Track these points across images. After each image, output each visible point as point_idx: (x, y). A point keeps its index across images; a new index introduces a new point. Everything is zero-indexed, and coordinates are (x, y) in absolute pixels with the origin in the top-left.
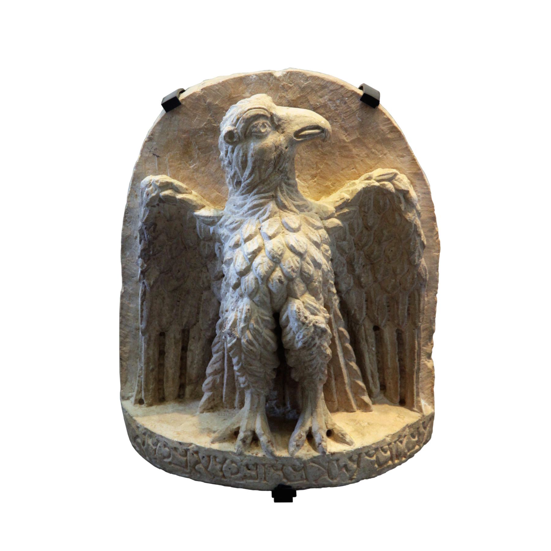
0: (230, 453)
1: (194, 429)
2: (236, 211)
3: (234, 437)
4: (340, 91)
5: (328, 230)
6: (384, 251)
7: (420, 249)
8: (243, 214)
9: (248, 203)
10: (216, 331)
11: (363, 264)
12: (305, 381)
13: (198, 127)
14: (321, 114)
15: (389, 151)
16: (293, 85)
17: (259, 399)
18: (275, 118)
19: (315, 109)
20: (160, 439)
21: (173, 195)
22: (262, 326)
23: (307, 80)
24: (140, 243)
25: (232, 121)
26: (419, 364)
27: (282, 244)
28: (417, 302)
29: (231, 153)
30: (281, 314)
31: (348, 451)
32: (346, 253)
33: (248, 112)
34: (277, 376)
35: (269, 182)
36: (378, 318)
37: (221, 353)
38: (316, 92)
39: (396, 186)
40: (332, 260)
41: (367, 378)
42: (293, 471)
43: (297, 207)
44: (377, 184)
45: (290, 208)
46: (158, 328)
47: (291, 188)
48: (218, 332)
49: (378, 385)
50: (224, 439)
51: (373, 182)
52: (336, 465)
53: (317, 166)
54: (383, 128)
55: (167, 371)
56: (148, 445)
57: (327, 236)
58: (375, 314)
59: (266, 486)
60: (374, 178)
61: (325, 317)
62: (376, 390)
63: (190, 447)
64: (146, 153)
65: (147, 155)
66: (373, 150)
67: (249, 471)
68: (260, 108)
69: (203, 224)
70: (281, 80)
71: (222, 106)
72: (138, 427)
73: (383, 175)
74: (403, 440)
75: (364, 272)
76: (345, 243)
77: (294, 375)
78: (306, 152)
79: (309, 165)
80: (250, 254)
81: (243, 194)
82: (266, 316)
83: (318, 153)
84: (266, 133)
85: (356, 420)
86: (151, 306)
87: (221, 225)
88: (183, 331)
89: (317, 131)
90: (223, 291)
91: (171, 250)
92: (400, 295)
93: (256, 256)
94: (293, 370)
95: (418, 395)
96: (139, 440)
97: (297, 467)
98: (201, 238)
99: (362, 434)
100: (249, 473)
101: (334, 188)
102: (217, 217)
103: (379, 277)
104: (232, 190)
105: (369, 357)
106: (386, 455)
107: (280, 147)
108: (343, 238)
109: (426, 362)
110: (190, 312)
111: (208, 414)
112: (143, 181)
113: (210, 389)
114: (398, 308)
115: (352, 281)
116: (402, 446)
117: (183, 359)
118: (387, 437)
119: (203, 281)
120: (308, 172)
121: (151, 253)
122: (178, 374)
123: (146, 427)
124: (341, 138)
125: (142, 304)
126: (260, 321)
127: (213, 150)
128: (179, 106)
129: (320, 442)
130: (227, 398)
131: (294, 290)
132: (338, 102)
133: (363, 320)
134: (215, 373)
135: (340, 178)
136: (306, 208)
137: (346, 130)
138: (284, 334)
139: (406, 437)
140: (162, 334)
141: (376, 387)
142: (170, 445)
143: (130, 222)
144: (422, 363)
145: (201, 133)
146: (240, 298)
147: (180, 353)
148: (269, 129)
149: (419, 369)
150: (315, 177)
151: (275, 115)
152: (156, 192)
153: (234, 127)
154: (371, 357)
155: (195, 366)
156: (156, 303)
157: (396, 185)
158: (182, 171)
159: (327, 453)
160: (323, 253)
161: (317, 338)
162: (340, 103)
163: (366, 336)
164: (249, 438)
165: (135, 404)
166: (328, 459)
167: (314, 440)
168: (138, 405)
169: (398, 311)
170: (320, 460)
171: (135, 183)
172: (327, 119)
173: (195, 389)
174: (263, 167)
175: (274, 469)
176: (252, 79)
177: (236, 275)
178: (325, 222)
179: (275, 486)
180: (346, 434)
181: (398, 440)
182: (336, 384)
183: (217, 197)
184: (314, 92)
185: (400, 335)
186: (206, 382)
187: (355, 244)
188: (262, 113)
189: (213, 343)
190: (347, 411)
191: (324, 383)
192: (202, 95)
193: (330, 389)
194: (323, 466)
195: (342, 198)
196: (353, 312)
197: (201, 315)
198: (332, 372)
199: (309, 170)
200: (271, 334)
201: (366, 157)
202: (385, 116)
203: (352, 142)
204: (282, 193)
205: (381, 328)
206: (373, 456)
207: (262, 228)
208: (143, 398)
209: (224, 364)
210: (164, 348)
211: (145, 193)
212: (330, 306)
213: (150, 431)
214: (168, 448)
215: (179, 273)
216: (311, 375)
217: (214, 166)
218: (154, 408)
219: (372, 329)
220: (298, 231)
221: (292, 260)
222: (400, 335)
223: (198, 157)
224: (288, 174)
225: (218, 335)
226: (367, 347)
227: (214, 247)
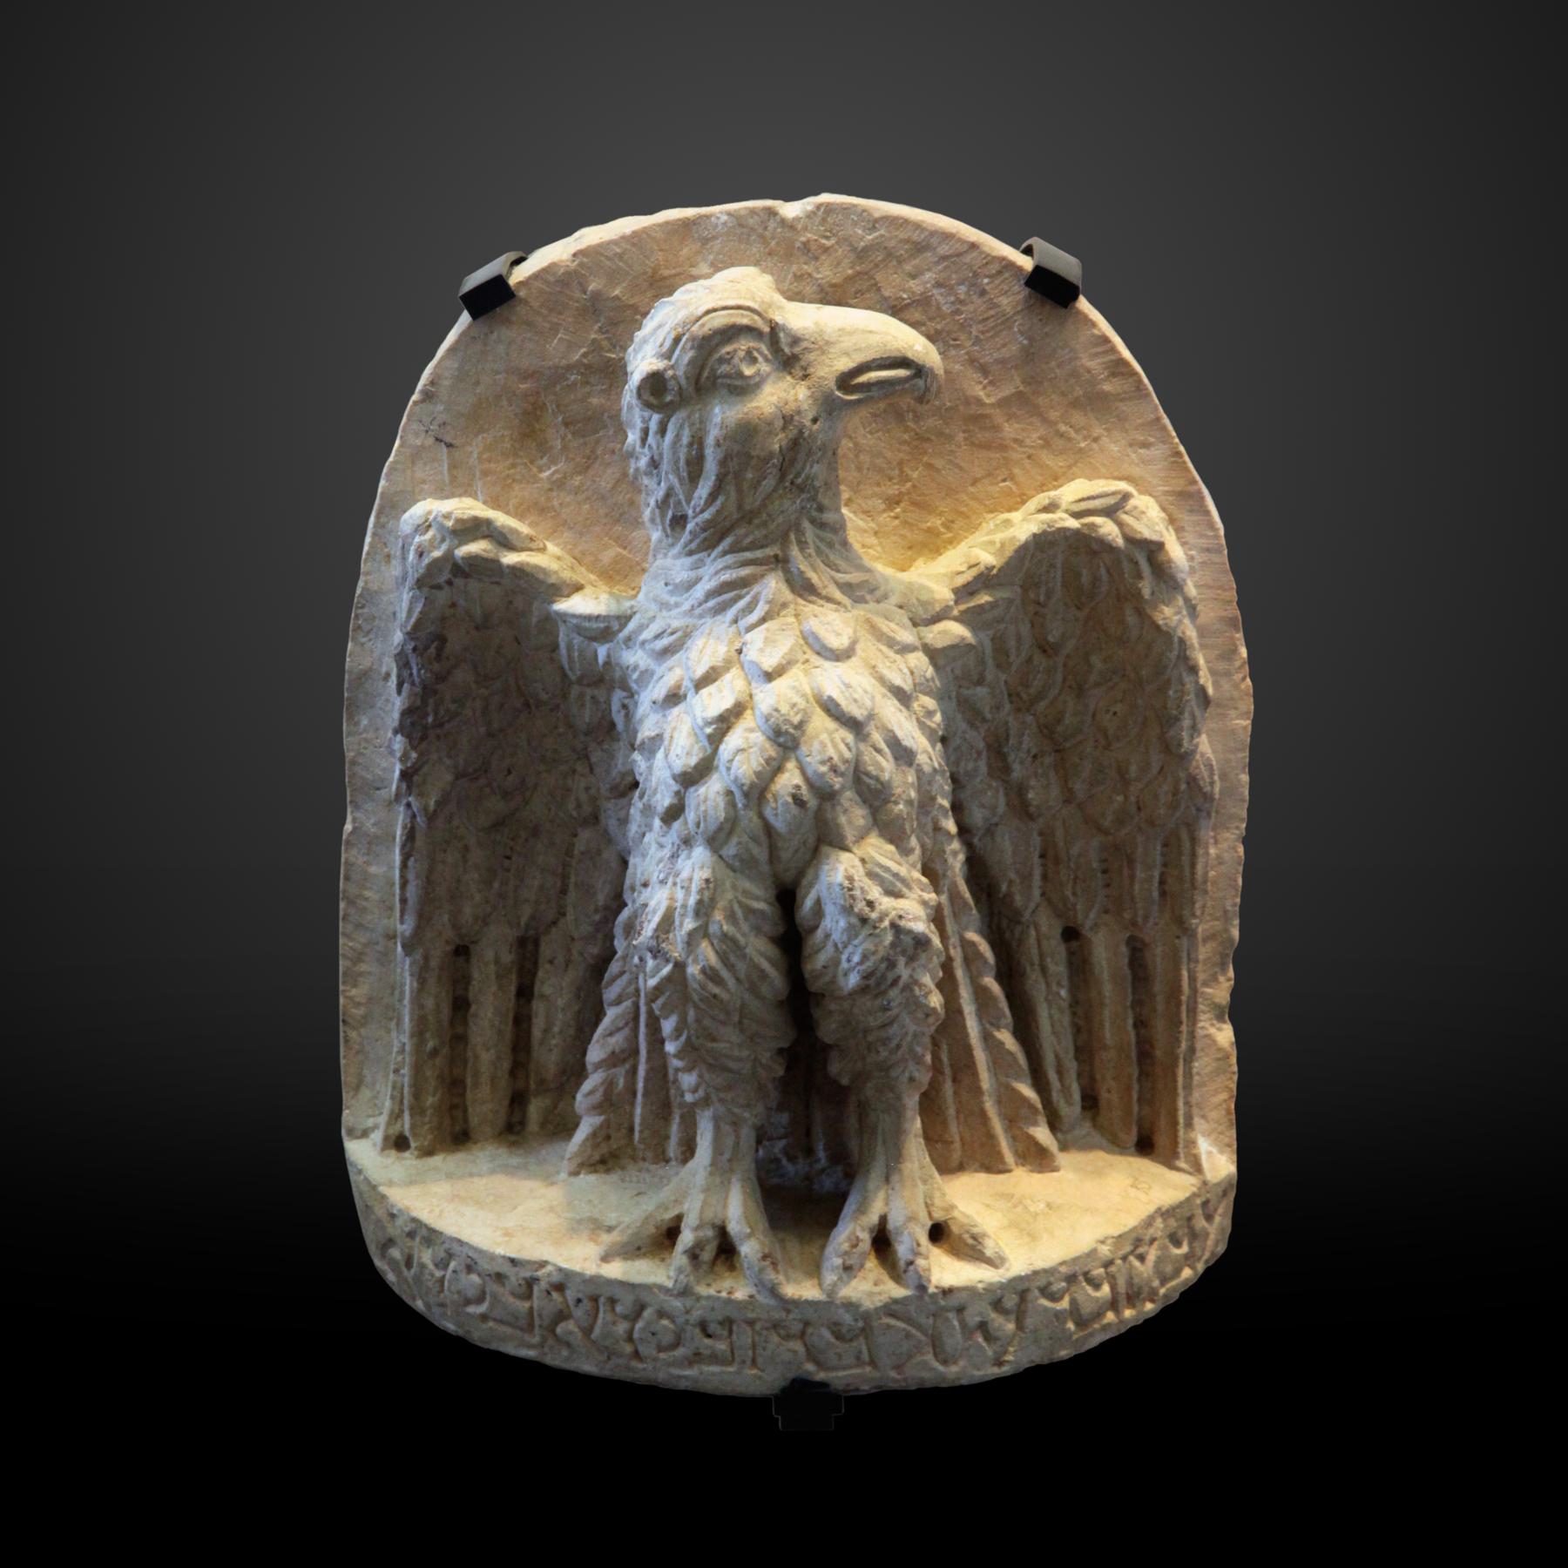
0: (656, 1290)
1: (552, 1220)
2: (673, 600)
3: (667, 1242)
4: (967, 259)
5: (932, 654)
6: (1094, 715)
7: (1196, 709)
8: (693, 608)
9: (706, 578)
10: (616, 943)
11: (1034, 751)
12: (869, 1085)
13: (564, 362)
14: (914, 325)
15: (1107, 430)
16: (833, 241)
17: (738, 1137)
18: (782, 335)
19: (896, 310)
20: (456, 1248)
21: (491, 555)
22: (745, 927)
23: (874, 227)
24: (399, 692)
25: (661, 345)
26: (1192, 1035)
27: (804, 695)
28: (1185, 859)
29: (659, 437)
30: (800, 893)
32: (984, 720)
33: (705, 319)
34: (788, 1069)
35: (764, 517)
36: (1074, 905)
37: (628, 1004)
39: (1127, 530)
40: (944, 740)
41: (1046, 1076)
42: (833, 1340)
43: (846, 588)
44: (1073, 523)
45: (824, 593)
46: (449, 933)
47: (828, 535)
49: (1077, 1097)
50: (639, 1248)
51: (1062, 519)
52: (956, 1323)
53: (902, 471)
54: (1090, 364)
55: (476, 1057)
56: (423, 1266)
57: (930, 672)
58: (1068, 893)
59: (758, 1382)
60: (1064, 506)
61: (924, 903)
62: (1071, 1109)
63: (540, 1273)
64: (417, 435)
65: (418, 442)
66: (1063, 428)
67: (707, 1341)
68: (739, 307)
69: (577, 637)
70: (800, 227)
71: (631, 302)
72: (393, 1216)
73: (1089, 498)
74: (1147, 1253)
75: (1036, 774)
76: (981, 691)
77: (837, 1068)
78: (871, 433)
79: (880, 471)
80: (710, 724)
81: (690, 553)
82: (757, 898)
83: (906, 437)
84: (757, 379)
85: (1013, 1196)
86: (431, 870)
87: (628, 639)
88: (522, 942)
89: (901, 373)
90: (633, 829)
91: (485, 710)
92: (1140, 839)
93: (729, 728)
94: (834, 1054)
95: (1189, 1125)
97: (844, 1330)
98: (573, 678)
99: (1029, 1234)
100: (707, 1347)
101: (949, 535)
102: (618, 618)
103: (1079, 787)
105: (1051, 1017)
106: (1098, 1294)
107: (796, 418)
108: (975, 678)
109: (1212, 1031)
110: (541, 888)
111: (592, 1178)
112: (406, 515)
113: (598, 1108)
114: (1132, 877)
115: (1002, 800)
116: (1144, 1270)
117: (522, 1021)
118: (1103, 1242)
119: (577, 799)
120: (876, 489)
121: (430, 719)
122: (506, 1065)
124: (969, 393)
125: (404, 865)
127: (605, 427)
128: (511, 303)
129: (911, 1257)
130: (647, 1133)
131: (838, 826)
132: (962, 289)
133: (1034, 912)
134: (613, 1060)
135: (967, 505)
136: (872, 591)
137: (984, 370)
138: (807, 951)
139: (1156, 1244)
140: (462, 951)
141: (1069, 1102)
142: (485, 1265)
144: (1200, 1032)
146: (683, 847)
147: (511, 1005)
149: (1192, 1050)
150: (898, 503)
151: (784, 328)
152: (444, 547)
153: (666, 362)
154: (1056, 1016)
155: (554, 1042)
156: (443, 862)
157: (1128, 525)
158: (517, 487)
159: (931, 1290)
160: (918, 720)
161: (902, 961)
162: (967, 293)
163: (1042, 956)
164: (708, 1248)
165: (383, 1149)
166: (932, 1307)
167: (895, 1252)
168: (393, 1152)
169: (1132, 884)
170: (912, 1308)
172: (930, 338)
173: (555, 1107)
174: (749, 475)
175: (779, 1335)
177: (672, 782)
178: (924, 630)
179: (784, 1384)
180: (984, 1235)
181: (1132, 1252)
182: (955, 1093)
183: (618, 560)
185: (1137, 953)
186: (587, 1086)
187: (1010, 695)
188: (745, 321)
190: (989, 1169)
191: (923, 1090)
192: (575, 272)
193: (940, 1108)
194: (919, 1327)
195: (972, 563)
196: (1004, 888)
198: (945, 1058)
199: (878, 485)
200: (772, 950)
201: (1042, 447)
202: (1096, 331)
203: (1002, 403)
204: (802, 550)
205: (1084, 932)
207: (744, 650)
208: (407, 1133)
209: (636, 1036)
211: (413, 548)
212: (940, 872)
213: (426, 1226)
214: (479, 1275)
215: (510, 778)
217: (609, 471)
218: (437, 1160)
219: (1059, 936)
220: (849, 657)
221: (832, 741)
222: (1137, 953)
223: (565, 448)
224: (820, 496)
225: (620, 954)
226: (1043, 986)
227: (608, 702)
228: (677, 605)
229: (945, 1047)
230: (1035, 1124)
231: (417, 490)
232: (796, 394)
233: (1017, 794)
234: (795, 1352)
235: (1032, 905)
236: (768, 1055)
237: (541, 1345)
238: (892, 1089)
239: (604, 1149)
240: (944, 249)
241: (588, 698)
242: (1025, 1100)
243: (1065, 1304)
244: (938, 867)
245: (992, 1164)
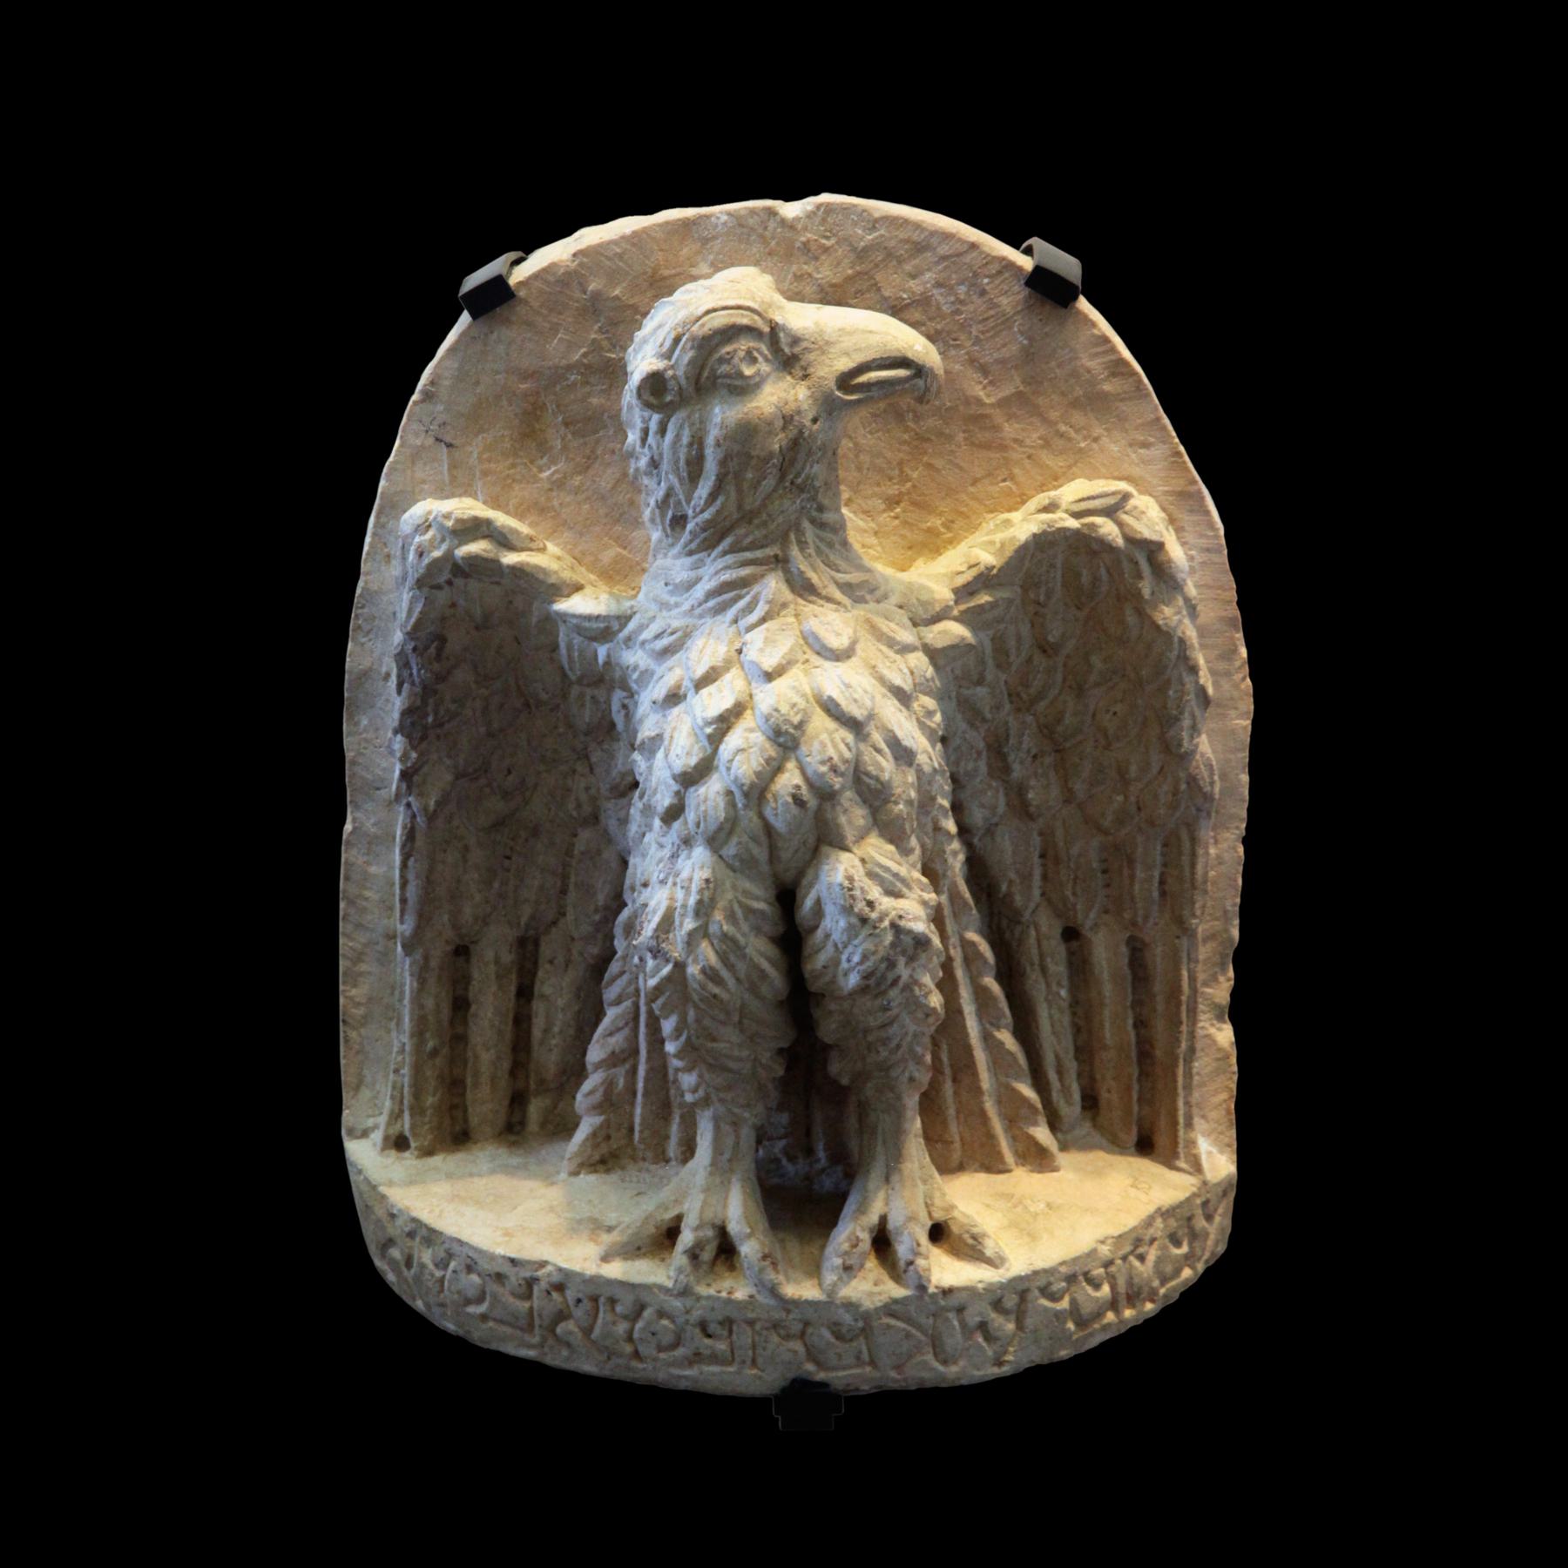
0: (656, 1290)
2: (673, 600)
3: (667, 1242)
4: (967, 259)
5: (932, 654)
6: (1094, 715)
7: (1196, 709)
8: (693, 608)
10: (616, 943)
11: (1034, 751)
12: (869, 1085)
13: (564, 362)
14: (914, 325)
15: (1107, 430)
16: (833, 241)
17: (738, 1137)
18: (782, 335)
19: (896, 310)
20: (456, 1248)
21: (491, 555)
22: (745, 927)
23: (874, 227)
24: (399, 692)
25: (661, 345)
26: (1192, 1035)
27: (804, 695)
28: (1185, 859)
29: (659, 437)
30: (800, 893)
32: (984, 720)
33: (705, 319)
34: (788, 1069)
35: (764, 517)
36: (1074, 905)
37: (628, 1004)
38: (900, 262)
39: (1127, 530)
41: (1046, 1076)
42: (833, 1340)
43: (846, 588)
44: (1073, 523)
45: (824, 593)
46: (449, 933)
47: (828, 535)
48: (620, 944)
49: (1077, 1097)
50: (639, 1248)
51: (1062, 519)
52: (956, 1323)
53: (902, 471)
54: (1090, 364)
55: (476, 1057)
56: (423, 1266)
57: (930, 672)
58: (1068, 893)
59: (758, 1382)
60: (1064, 506)
61: (924, 903)
62: (1071, 1109)
63: (540, 1273)
64: (417, 435)
65: (418, 442)
66: (1063, 428)
67: (707, 1341)
68: (739, 307)
69: (577, 637)
70: (800, 227)
71: (631, 302)
72: (393, 1216)
73: (1089, 498)
74: (1147, 1253)
75: (1036, 774)
76: (981, 691)
77: (837, 1068)
79: (880, 471)
80: (710, 724)
81: (690, 553)
82: (757, 898)
83: (906, 437)
84: (757, 379)
85: (1013, 1196)
86: (431, 870)
87: (628, 639)
88: (522, 942)
89: (901, 373)
90: (633, 829)
91: (485, 710)
92: (1140, 839)
93: (729, 728)
94: (834, 1054)
95: (1189, 1125)
97: (844, 1330)
98: (573, 678)
99: (1029, 1234)
100: (707, 1347)
101: (949, 535)
102: (618, 618)
103: (1079, 787)
105: (1051, 1017)
106: (1098, 1294)
107: (796, 418)
108: (975, 678)
109: (1212, 1031)
110: (541, 888)
111: (592, 1178)
112: (406, 515)
113: (598, 1108)
114: (1132, 877)
115: (1002, 800)
116: (1144, 1270)
117: (522, 1021)
118: (1103, 1242)
119: (577, 799)
120: (876, 489)
121: (430, 719)
122: (506, 1065)
123: (414, 1214)
124: (969, 393)
125: (404, 865)
126: (739, 913)
127: (605, 427)
128: (511, 303)
129: (911, 1257)
130: (647, 1133)
131: (838, 826)
133: (1034, 912)
134: (613, 1060)
135: (967, 505)
136: (872, 591)
137: (984, 370)
138: (807, 951)
139: (1156, 1244)
140: (462, 951)
141: (1069, 1102)
142: (485, 1265)
143: (369, 632)
144: (1200, 1032)
146: (683, 847)
147: (511, 1005)
148: (765, 367)
149: (1192, 1050)
150: (898, 503)
151: (784, 328)
152: (444, 547)
153: (666, 362)
155: (554, 1042)
156: (443, 862)
157: (1128, 525)
158: (517, 487)
159: (931, 1290)
160: (918, 720)
161: (902, 961)
162: (967, 293)
163: (1042, 956)
164: (708, 1248)
165: (383, 1149)
166: (932, 1307)
167: (895, 1252)
168: (393, 1152)
169: (1132, 884)
170: (912, 1308)
171: (383, 520)
173: (555, 1107)
174: (749, 475)
177: (672, 782)
178: (924, 630)
179: (784, 1384)
180: (984, 1235)
181: (1132, 1252)
182: (955, 1093)
183: (618, 560)
185: (1137, 953)
186: (587, 1086)
187: (1010, 695)
188: (745, 321)
190: (989, 1169)
191: (923, 1090)
192: (575, 272)
193: (940, 1108)
194: (919, 1327)
195: (972, 563)
196: (1004, 888)
198: (945, 1058)
199: (878, 485)
200: (772, 950)
201: (1042, 447)
202: (1096, 331)
203: (1002, 403)
204: (802, 550)
205: (1084, 932)
206: (1061, 1298)
207: (744, 650)
208: (407, 1133)
209: (636, 1036)
211: (413, 548)
212: (940, 872)
213: (426, 1226)
214: (479, 1275)
215: (510, 778)
217: (609, 471)
218: (437, 1160)
219: (1059, 936)
220: (849, 657)
221: (832, 741)
222: (1137, 953)
223: (565, 448)
224: (820, 496)
225: (620, 954)
226: (1043, 986)
227: (608, 702)
231: (417, 490)
232: (796, 394)
233: (1017, 794)
234: (795, 1352)
237: (541, 1345)
238: (892, 1089)
239: (604, 1149)
240: (944, 249)
241: (588, 698)
242: (1025, 1100)
244: (938, 867)
245: (992, 1164)
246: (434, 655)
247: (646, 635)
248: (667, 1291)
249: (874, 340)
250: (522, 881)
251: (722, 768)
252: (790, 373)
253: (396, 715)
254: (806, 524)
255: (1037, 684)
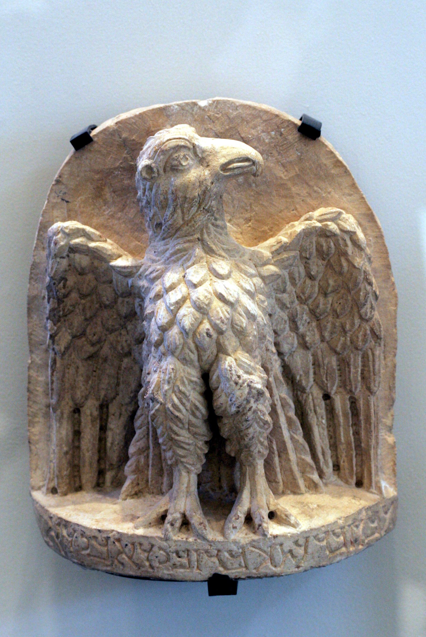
0: (157, 539)
1: (115, 516)
2: (158, 258)
3: (162, 522)
4: (274, 121)
5: (263, 278)
6: (332, 305)
7: (372, 300)
8: (165, 260)
9: (170, 248)
10: (139, 403)
11: (308, 321)
12: (242, 455)
13: (112, 167)
14: (255, 148)
15: (333, 189)
16: (220, 115)
17: (189, 478)
18: (198, 149)
19: (246, 141)
20: (77, 528)
21: (84, 243)
22: (189, 388)
23: (236, 109)
24: (49, 302)
25: (149, 154)
26: (377, 437)
27: (210, 293)
28: (371, 363)
29: (150, 191)
30: (211, 374)
31: (293, 534)
32: (287, 308)
33: (167, 143)
34: (209, 451)
35: (193, 222)
36: (327, 384)
37: (144, 428)
38: (247, 123)
39: (340, 227)
40: (270, 315)
41: (317, 456)
42: (230, 557)
43: (227, 251)
44: (319, 225)
45: (218, 253)
46: (71, 403)
47: (220, 230)
48: (140, 403)
49: (331, 465)
50: (150, 523)
51: (314, 223)
52: (280, 550)
53: (251, 207)
54: (325, 162)
55: (84, 454)
56: (63, 536)
57: (262, 285)
58: (324, 379)
59: (200, 576)
60: (315, 218)
61: (262, 378)
62: (329, 470)
63: (110, 535)
64: (54, 198)
65: (55, 201)
66: (316, 188)
67: (178, 559)
68: (180, 138)
69: (120, 276)
70: (207, 110)
71: (139, 141)
72: (51, 518)
73: (325, 214)
74: (359, 525)
75: (309, 330)
76: (285, 296)
77: (230, 449)
78: (238, 192)
79: (243, 207)
80: (172, 305)
81: (164, 239)
82: (194, 376)
83: (252, 193)
84: (188, 167)
85: (303, 503)
86: (64, 376)
87: (140, 275)
88: (101, 407)
89: (246, 164)
90: (144, 353)
91: (84, 310)
92: (352, 355)
93: (180, 307)
94: (228, 443)
95: (377, 475)
96: (53, 533)
97: (234, 553)
98: (119, 294)
99: (309, 516)
100: (179, 561)
101: (271, 233)
102: (136, 267)
103: (327, 334)
104: (152, 235)
105: (319, 432)
106: (338, 540)
107: (204, 182)
108: (282, 290)
109: (386, 437)
110: (109, 383)
111: (132, 501)
112: (50, 229)
113: (135, 471)
114: (350, 372)
115: (296, 342)
116: (359, 531)
117: (102, 440)
118: (340, 519)
119: (122, 346)
120: (241, 215)
121: (61, 313)
122: (96, 458)
123: (60, 516)
124: (278, 175)
125: (52, 375)
126: (186, 382)
127: (130, 192)
128: (91, 143)
129: (260, 523)
130: (154, 482)
131: (225, 346)
132: (273, 133)
133: (311, 388)
134: (140, 451)
135: (278, 221)
136: (238, 252)
137: (283, 166)
138: (215, 398)
139: (363, 522)
140: (77, 410)
141: (328, 467)
142: (88, 533)
143: (36, 280)
144: (380, 437)
145: (116, 173)
146: (163, 357)
147: (98, 433)
148: (191, 162)
149: (377, 443)
150: (250, 220)
151: (198, 146)
152: (65, 241)
153: (151, 161)
154: (322, 431)
155: (115, 448)
156: (68, 373)
157: (341, 225)
158: (95, 218)
159: (269, 536)
160: (258, 304)
161: (252, 401)
162: (275, 134)
163: (314, 406)
164: (178, 521)
165: (46, 494)
166: (269, 543)
167: (254, 522)
168: (51, 495)
169: (349, 375)
170: (261, 544)
171: (41, 233)
172: (262, 154)
173: (117, 476)
174: (186, 206)
175: (207, 556)
176: (173, 110)
177: (157, 330)
178: (260, 269)
179: (210, 576)
180: (290, 515)
181: (352, 524)
182: (280, 462)
183: (136, 246)
184: (245, 123)
185: (354, 402)
186: (129, 463)
187: (297, 297)
188: (183, 144)
189: (136, 417)
190: (295, 493)
191: (265, 458)
192: (117, 130)
193: (273, 468)
194: (265, 552)
195: (279, 241)
196: (298, 378)
197: (122, 386)
198: (275, 447)
199: (242, 213)
200: (200, 398)
201: (307, 196)
202: (327, 149)
203: (291, 179)
204: (209, 236)
205: (331, 396)
206: (323, 540)
207: (186, 276)
208: (56, 487)
209: (148, 441)
210: (79, 427)
211: (53, 242)
212: (270, 368)
213: (64, 520)
214: (86, 538)
215: (95, 337)
216: (247, 447)
217: (132, 211)
218: (69, 497)
219: (321, 398)
220: (228, 278)
221: (222, 311)
222: (354, 402)
223: (114, 202)
224: (215, 214)
225: (140, 407)
226: (315, 419)
227: (133, 304)
228: (159, 260)
229: (274, 442)
230: (313, 474)
231: (55, 220)
232: (204, 173)
233: (302, 337)
234: (214, 563)
235: (310, 385)
236: (201, 443)
237: (112, 565)
238: (251, 456)
239: (136, 489)
240: (265, 117)
241: (125, 302)
242: (308, 464)
243: (324, 543)
244: (269, 366)
245: (295, 491)
246: (62, 286)
247: (147, 273)
248: (161, 539)
249: (235, 151)
250: (100, 380)
251: (178, 323)
252: (202, 165)
253: (47, 312)
254: (210, 225)
255: (308, 292)
